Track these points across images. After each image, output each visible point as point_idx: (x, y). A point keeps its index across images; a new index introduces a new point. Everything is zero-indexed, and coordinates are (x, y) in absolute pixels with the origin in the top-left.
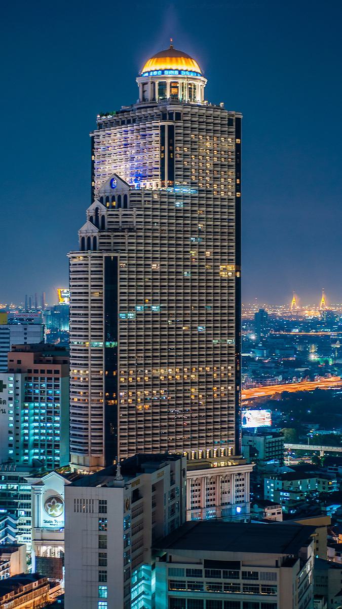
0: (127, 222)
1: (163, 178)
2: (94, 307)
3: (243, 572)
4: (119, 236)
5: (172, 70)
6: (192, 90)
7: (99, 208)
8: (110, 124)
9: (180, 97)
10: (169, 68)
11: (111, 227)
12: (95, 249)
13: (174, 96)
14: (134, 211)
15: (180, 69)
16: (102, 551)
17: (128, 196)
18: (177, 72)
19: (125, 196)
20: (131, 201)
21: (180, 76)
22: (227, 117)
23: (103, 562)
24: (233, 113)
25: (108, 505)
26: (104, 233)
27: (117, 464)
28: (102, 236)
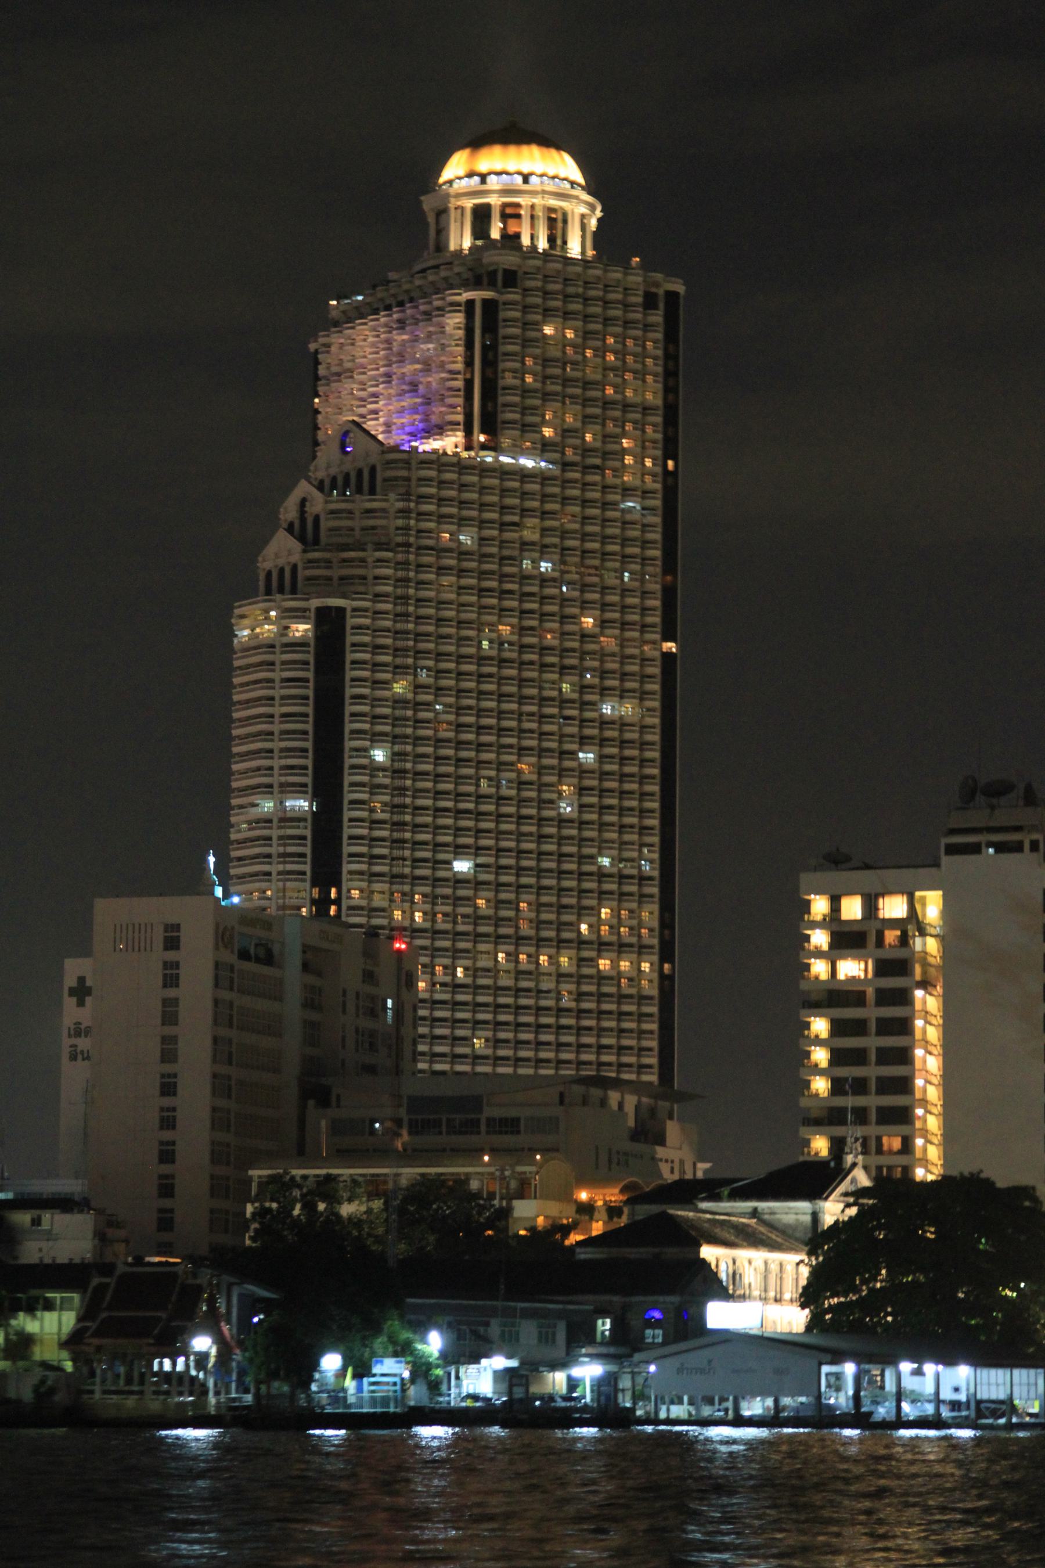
0: (373, 528)
1: (468, 432)
2: (288, 732)
3: (488, 1119)
4: (352, 560)
5: (507, 173)
6: (556, 223)
7: (309, 497)
8: (361, 313)
9: (526, 241)
10: (498, 167)
11: (334, 540)
12: (294, 590)
13: (511, 240)
14: (392, 500)
15: (526, 171)
16: (169, 1030)
17: (379, 469)
18: (519, 179)
19: (373, 470)
20: (385, 480)
21: (526, 187)
22: (642, 287)
23: (169, 1054)
24: (659, 276)
25: (182, 934)
26: (316, 555)
27: (375, 1188)
28: (310, 561)
